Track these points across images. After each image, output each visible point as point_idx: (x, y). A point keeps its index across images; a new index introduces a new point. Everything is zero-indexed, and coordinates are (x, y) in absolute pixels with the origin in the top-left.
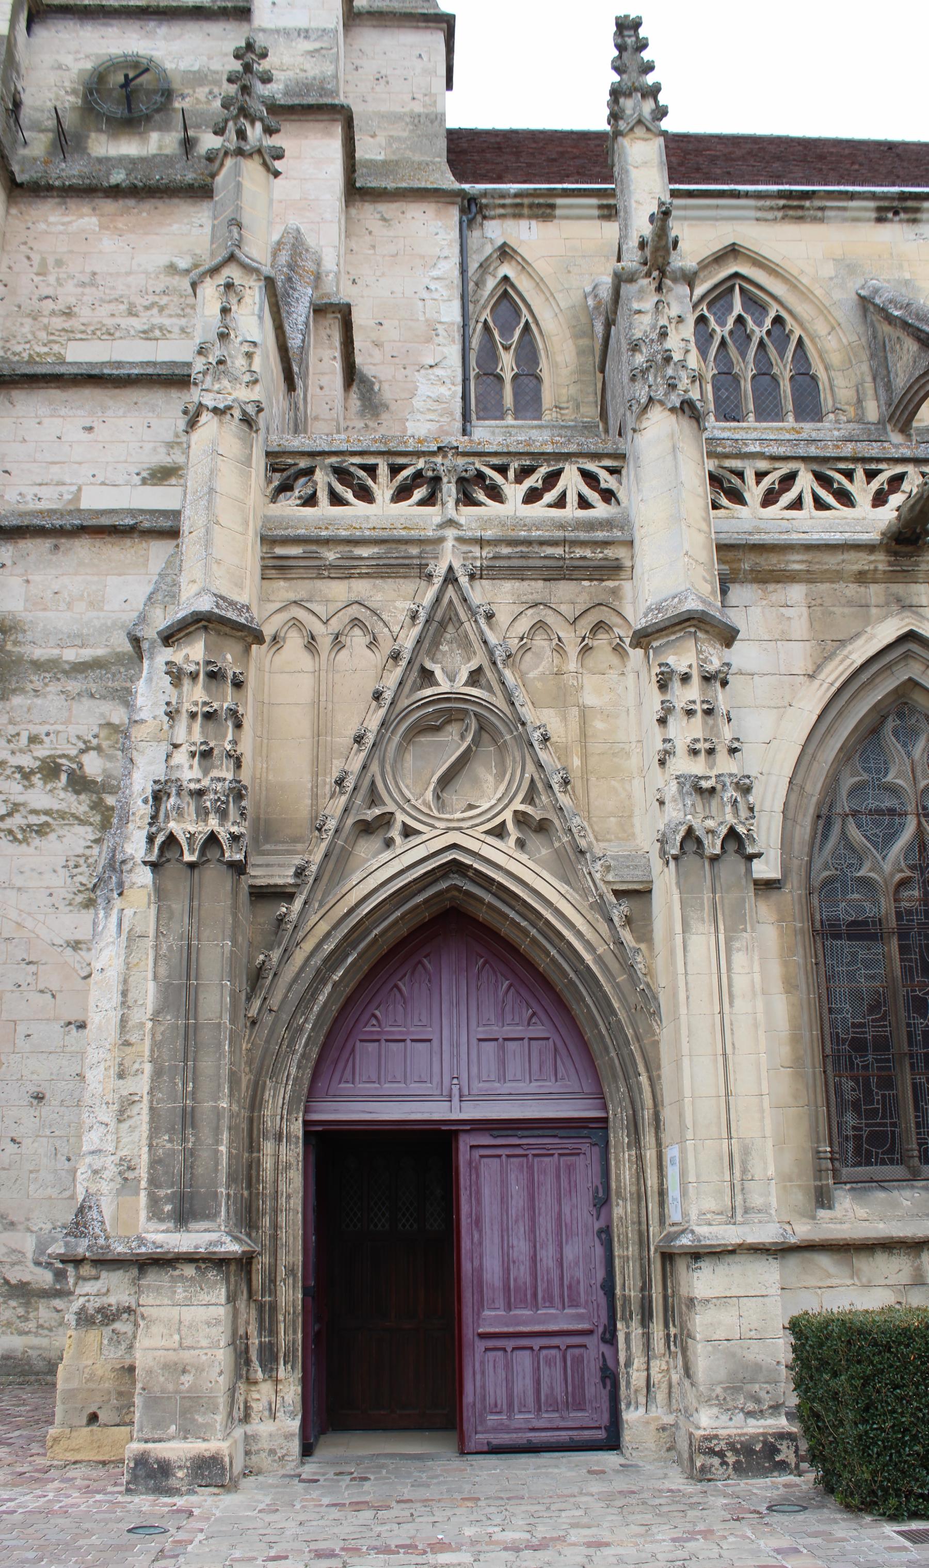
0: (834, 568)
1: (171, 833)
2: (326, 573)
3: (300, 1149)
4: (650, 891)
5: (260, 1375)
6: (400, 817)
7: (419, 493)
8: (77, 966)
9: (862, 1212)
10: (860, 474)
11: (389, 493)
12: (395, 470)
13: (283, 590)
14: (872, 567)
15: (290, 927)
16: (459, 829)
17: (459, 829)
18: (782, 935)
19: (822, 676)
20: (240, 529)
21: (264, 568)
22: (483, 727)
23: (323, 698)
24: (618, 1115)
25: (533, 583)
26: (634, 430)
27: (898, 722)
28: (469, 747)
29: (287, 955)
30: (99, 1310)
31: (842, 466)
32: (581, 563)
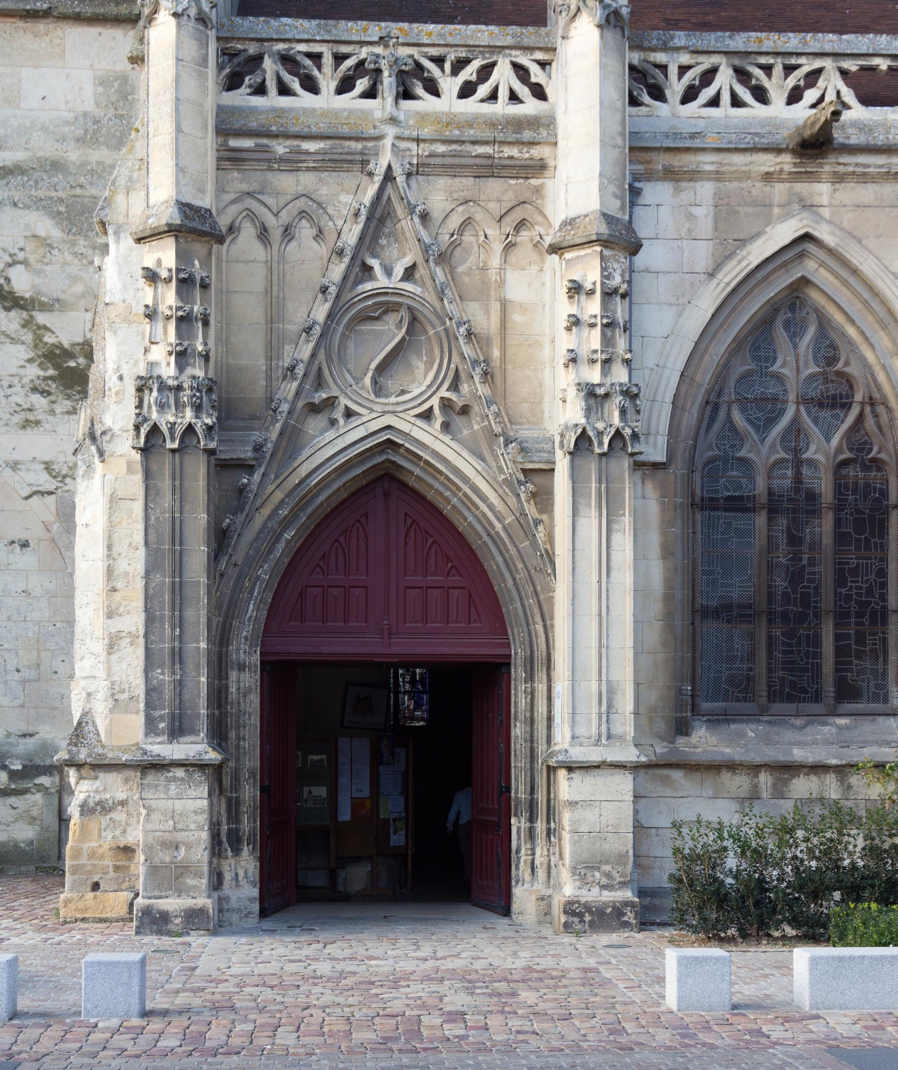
0: (742, 168)
1: (155, 424)
2: (276, 166)
3: (258, 677)
4: (553, 470)
5: (230, 853)
6: (343, 401)
7: (362, 85)
8: (18, 487)
9: (713, 740)
10: (778, 70)
11: (333, 85)
12: (339, 58)
13: (238, 181)
14: (778, 168)
15: (251, 496)
16: (393, 412)
17: (393, 412)
18: (663, 509)
19: (720, 276)
20: (200, 134)
21: (219, 159)
22: (414, 322)
23: (275, 289)
24: (518, 653)
25: (464, 180)
26: (563, 38)
27: (790, 315)
28: (403, 339)
29: (249, 519)
30: (99, 803)
31: (763, 60)
32: (508, 162)
